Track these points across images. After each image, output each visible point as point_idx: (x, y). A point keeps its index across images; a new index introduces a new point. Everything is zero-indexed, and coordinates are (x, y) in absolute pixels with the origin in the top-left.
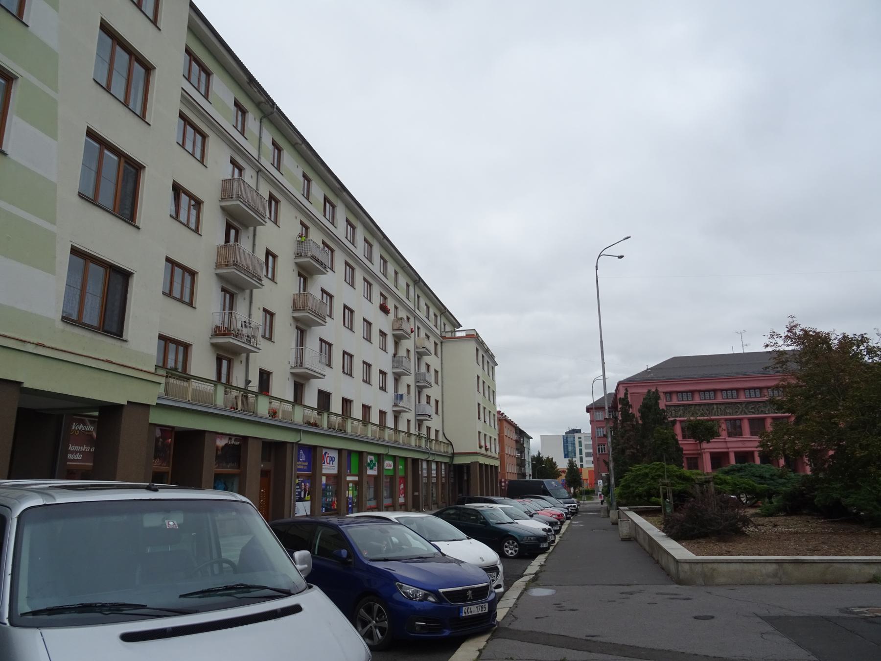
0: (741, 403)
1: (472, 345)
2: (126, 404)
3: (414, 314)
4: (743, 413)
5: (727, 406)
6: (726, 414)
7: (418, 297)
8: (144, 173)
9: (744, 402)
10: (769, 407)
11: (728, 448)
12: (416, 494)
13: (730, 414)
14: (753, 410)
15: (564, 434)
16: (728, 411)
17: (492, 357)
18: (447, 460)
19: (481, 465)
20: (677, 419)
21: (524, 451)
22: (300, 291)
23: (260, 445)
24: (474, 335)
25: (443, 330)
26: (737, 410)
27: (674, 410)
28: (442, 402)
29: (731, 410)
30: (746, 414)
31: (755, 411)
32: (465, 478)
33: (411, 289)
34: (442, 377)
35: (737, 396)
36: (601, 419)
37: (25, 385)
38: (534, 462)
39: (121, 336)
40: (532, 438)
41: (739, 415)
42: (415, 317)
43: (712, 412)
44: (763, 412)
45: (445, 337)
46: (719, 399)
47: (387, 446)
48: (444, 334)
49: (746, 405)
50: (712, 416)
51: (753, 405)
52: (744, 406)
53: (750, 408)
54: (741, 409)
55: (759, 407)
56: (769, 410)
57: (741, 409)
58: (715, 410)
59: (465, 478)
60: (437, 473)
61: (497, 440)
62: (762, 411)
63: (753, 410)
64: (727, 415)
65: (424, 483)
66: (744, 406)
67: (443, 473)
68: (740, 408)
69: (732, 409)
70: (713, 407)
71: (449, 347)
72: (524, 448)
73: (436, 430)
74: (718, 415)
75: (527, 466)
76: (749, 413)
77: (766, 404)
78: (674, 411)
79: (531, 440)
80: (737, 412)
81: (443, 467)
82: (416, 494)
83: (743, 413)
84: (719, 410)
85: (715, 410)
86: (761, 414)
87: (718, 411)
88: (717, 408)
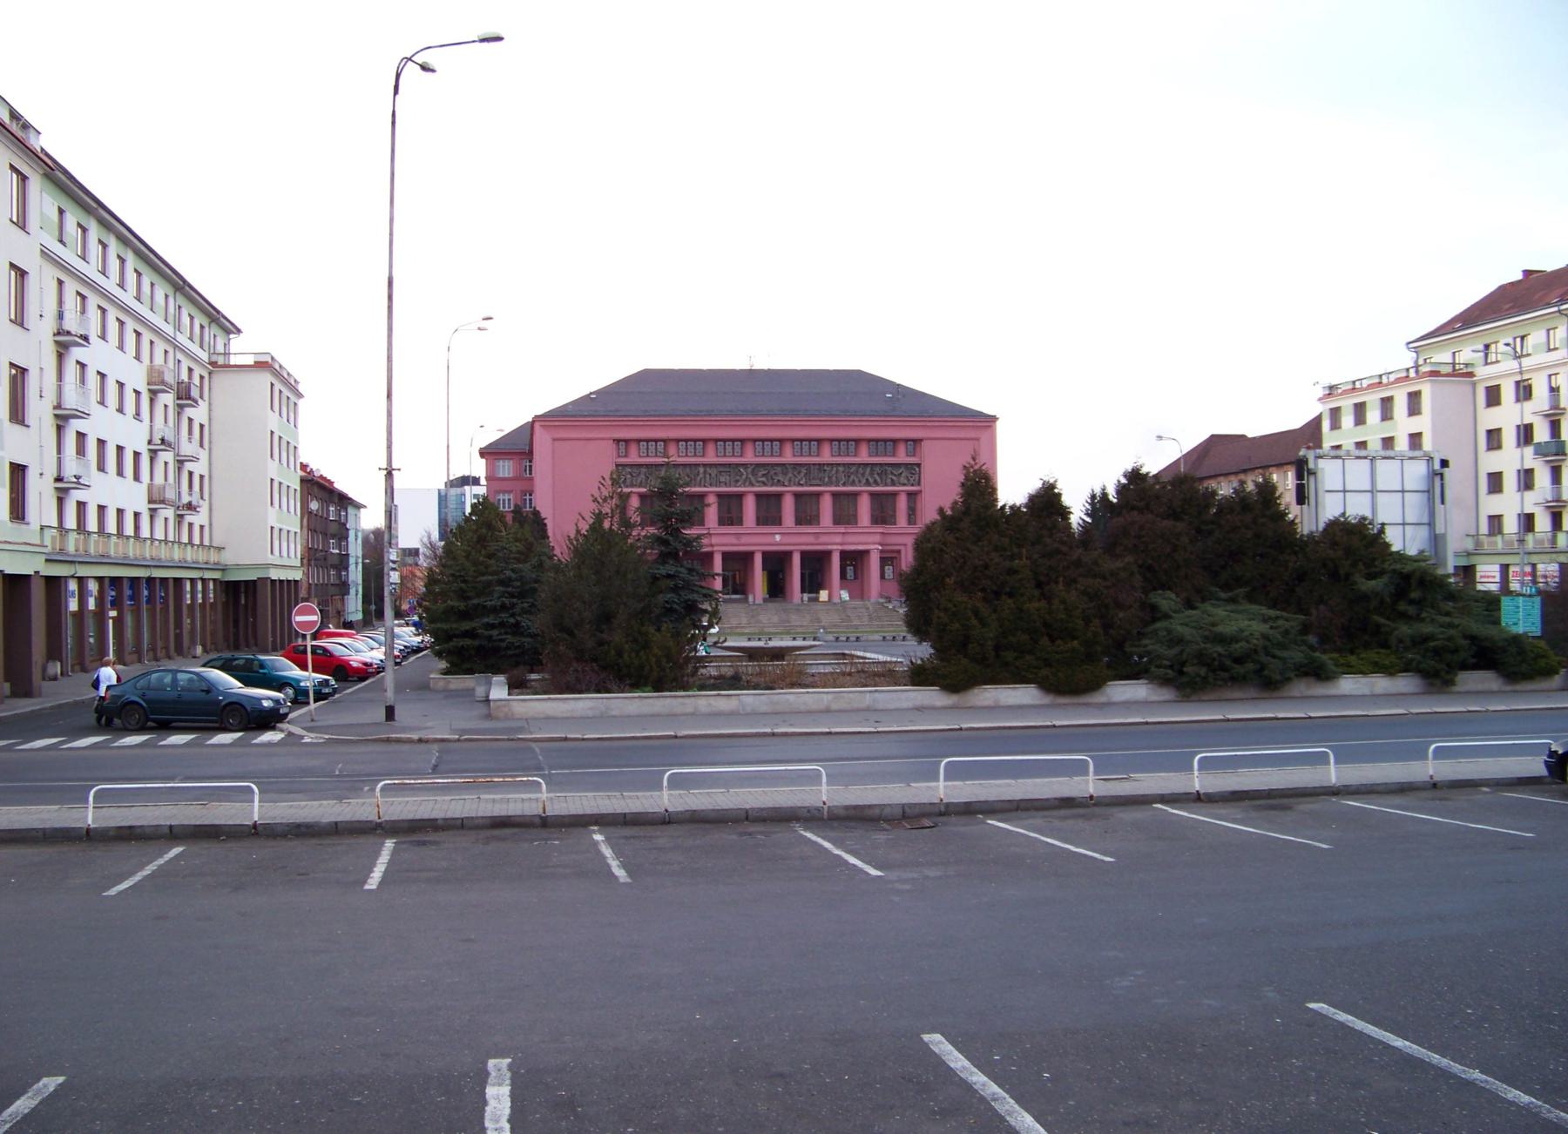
0: (745, 465)
1: (266, 378)
2: (33, 573)
3: (174, 344)
4: (747, 484)
5: (721, 469)
6: (719, 484)
7: (180, 307)
8: (28, 375)
9: (751, 464)
10: (790, 475)
11: (712, 546)
12: (178, 631)
13: (726, 484)
14: (764, 479)
15: (443, 487)
16: (722, 479)
17: (293, 388)
18: (217, 575)
19: (273, 581)
20: (634, 490)
21: (347, 538)
22: (166, 480)
23: (43, 582)
24: (267, 362)
25: (212, 351)
26: (738, 478)
27: (630, 474)
28: (210, 477)
29: (728, 478)
30: (753, 485)
31: (767, 480)
32: (243, 602)
33: (171, 300)
34: (210, 434)
35: (742, 452)
36: (507, 476)
37: (6, 572)
38: (368, 561)
39: (23, 519)
40: (365, 507)
41: (740, 486)
42: (175, 347)
43: (695, 480)
44: (779, 483)
45: (216, 362)
46: (711, 458)
47: (149, 566)
48: (214, 358)
49: (753, 470)
50: (695, 486)
51: (765, 470)
52: (750, 470)
53: (760, 474)
54: (744, 477)
55: (775, 473)
56: (790, 480)
57: (744, 477)
58: (701, 476)
59: (243, 602)
60: (203, 598)
61: (299, 535)
62: (779, 481)
63: (764, 479)
64: (720, 486)
65: (509, 694)
66: (750, 470)
67: (212, 596)
68: (743, 474)
69: (730, 476)
70: (698, 472)
71: (222, 381)
72: (348, 530)
73: (98, 440)
74: (705, 486)
75: (352, 568)
76: (757, 484)
77: (786, 468)
78: (629, 476)
79: (362, 510)
80: (737, 481)
81: (211, 585)
82: (178, 631)
83: (747, 484)
84: (708, 476)
85: (701, 476)
86: (777, 486)
87: (705, 477)
88: (705, 472)
